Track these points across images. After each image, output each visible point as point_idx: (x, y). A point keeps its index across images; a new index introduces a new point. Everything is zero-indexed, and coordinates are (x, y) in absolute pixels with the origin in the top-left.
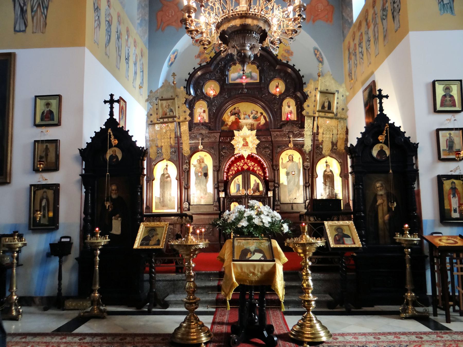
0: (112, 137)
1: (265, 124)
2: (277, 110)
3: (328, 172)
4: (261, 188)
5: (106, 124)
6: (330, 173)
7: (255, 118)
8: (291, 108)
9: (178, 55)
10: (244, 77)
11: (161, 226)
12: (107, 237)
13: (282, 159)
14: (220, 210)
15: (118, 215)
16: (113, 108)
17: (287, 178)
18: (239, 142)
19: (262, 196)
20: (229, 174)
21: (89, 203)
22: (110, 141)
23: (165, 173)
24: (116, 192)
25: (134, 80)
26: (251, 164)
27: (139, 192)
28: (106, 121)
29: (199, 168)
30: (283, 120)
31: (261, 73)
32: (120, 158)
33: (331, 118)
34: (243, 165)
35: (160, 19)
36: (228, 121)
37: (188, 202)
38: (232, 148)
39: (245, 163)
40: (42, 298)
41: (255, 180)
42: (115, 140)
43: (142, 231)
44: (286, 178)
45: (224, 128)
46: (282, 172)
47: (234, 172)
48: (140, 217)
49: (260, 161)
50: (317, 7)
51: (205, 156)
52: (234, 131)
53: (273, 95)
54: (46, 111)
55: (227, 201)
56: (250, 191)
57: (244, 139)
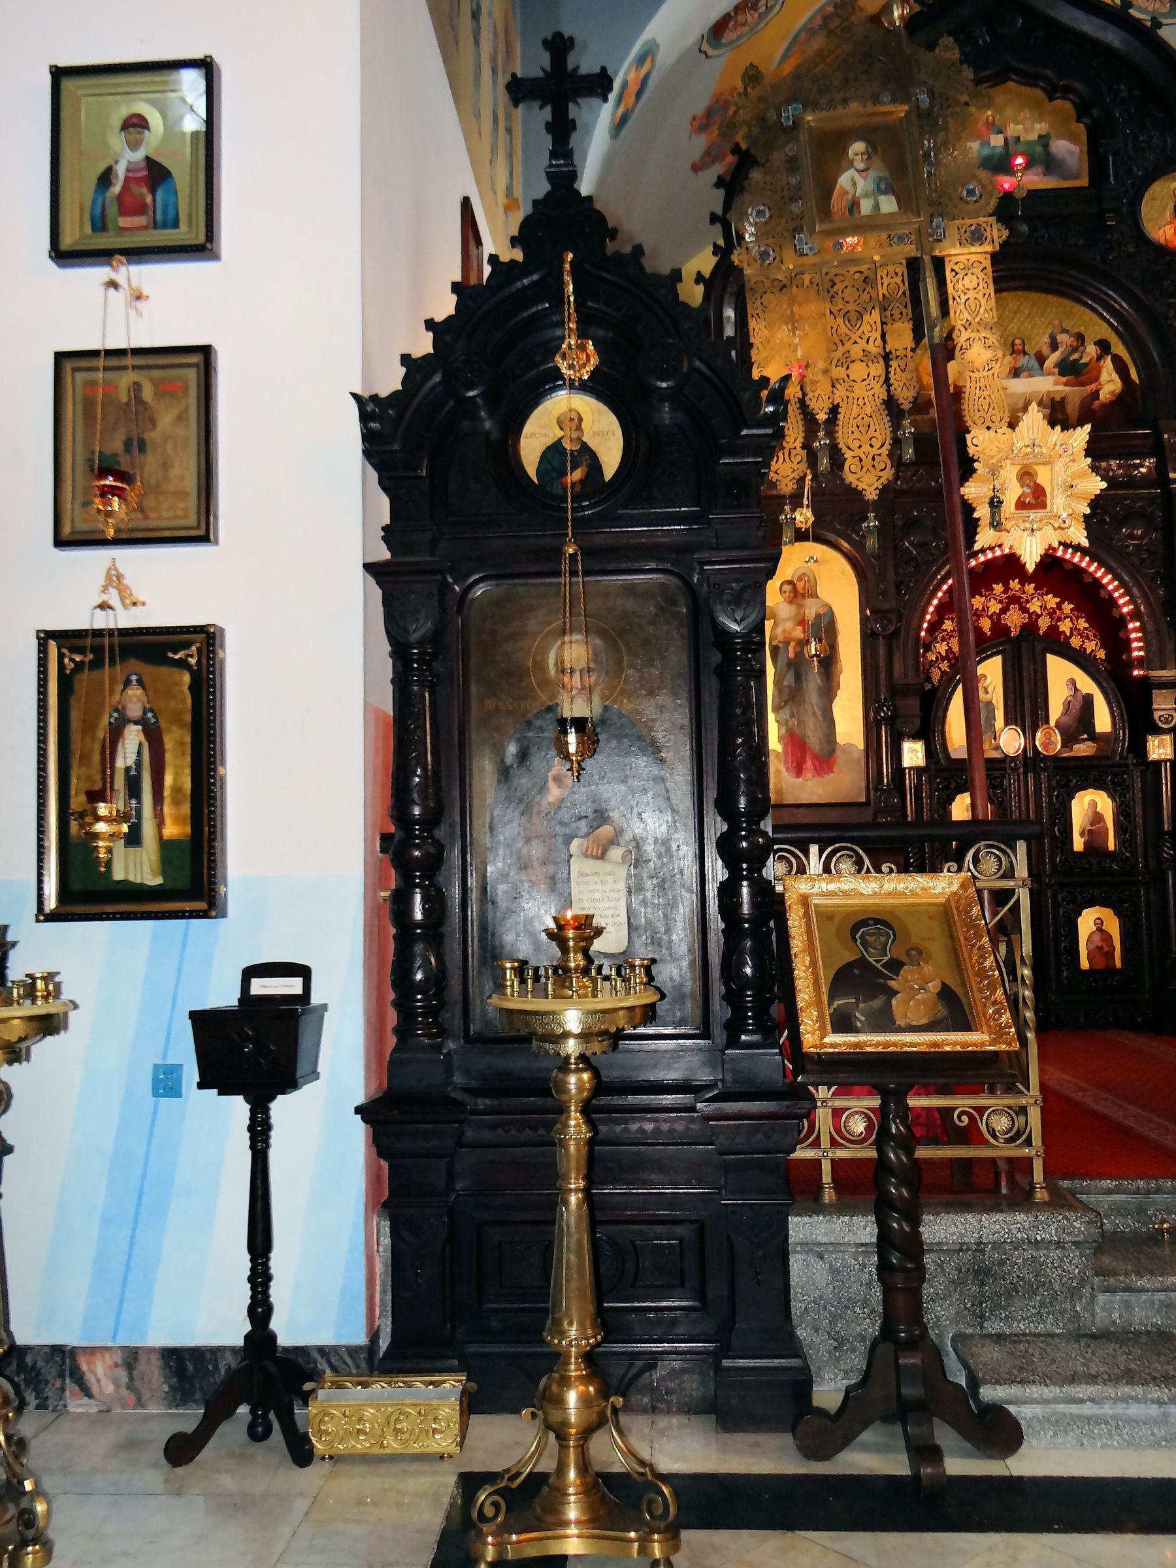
1: (1120, 400)
4: (1103, 721)
7: (1070, 369)
9: (654, 74)
19: (1108, 758)
21: (940, 600)
29: (789, 625)
34: (1004, 610)
39: (1014, 599)
40: (132, 1357)
41: (1073, 682)
49: (1097, 583)
54: (121, 170)
57: (1026, 475)
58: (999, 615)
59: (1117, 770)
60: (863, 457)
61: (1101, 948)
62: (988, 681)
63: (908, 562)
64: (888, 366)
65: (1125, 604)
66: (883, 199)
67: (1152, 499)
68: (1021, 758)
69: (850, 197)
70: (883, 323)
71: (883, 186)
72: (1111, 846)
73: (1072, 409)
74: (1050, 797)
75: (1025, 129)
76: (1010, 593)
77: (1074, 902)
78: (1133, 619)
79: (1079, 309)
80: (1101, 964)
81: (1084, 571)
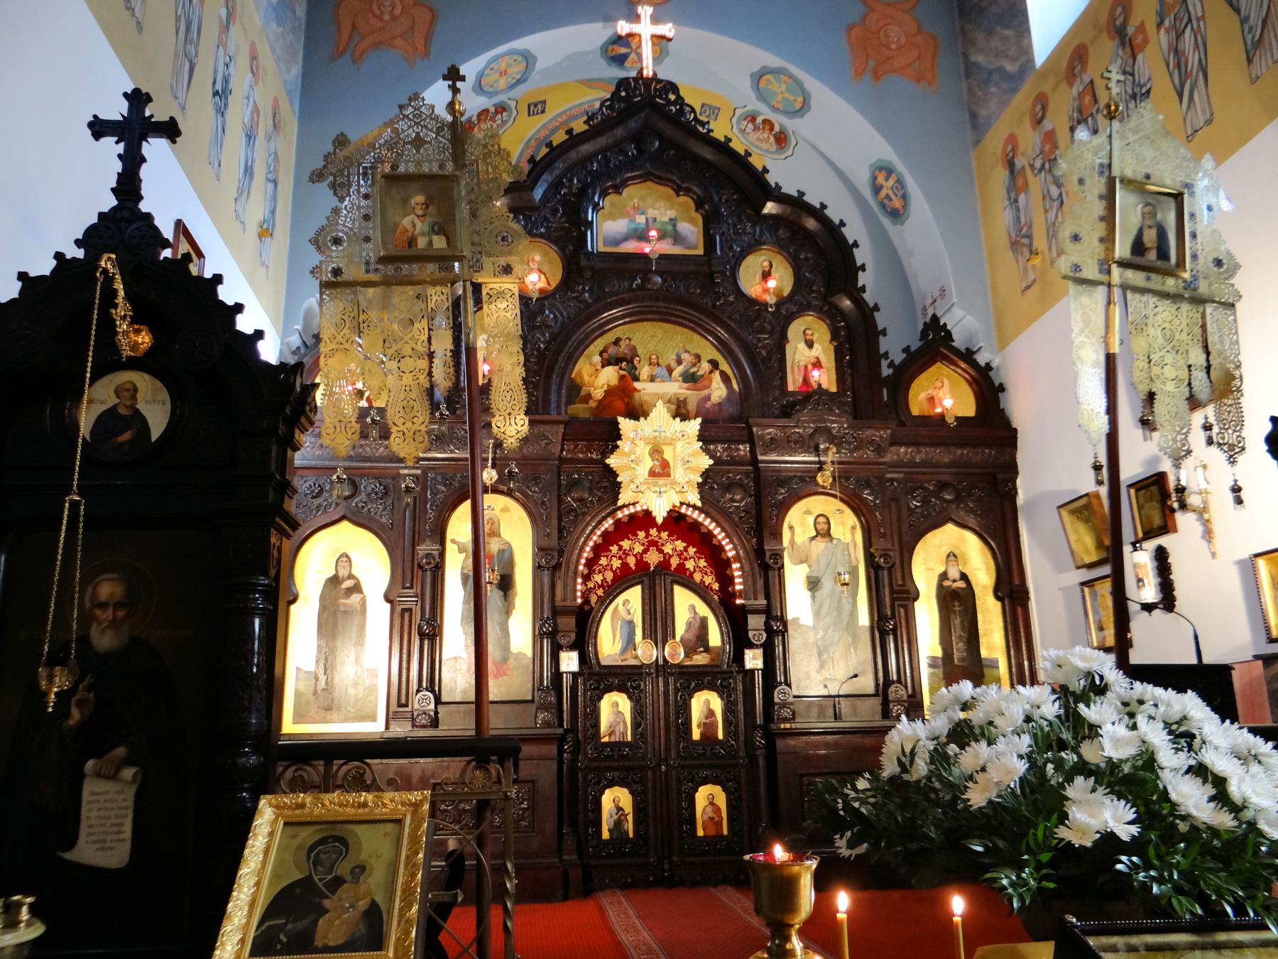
0: (122, 308)
2: (768, 353)
3: (954, 581)
4: (715, 638)
5: (91, 240)
6: (961, 584)
7: (691, 378)
8: (818, 351)
10: (653, 233)
11: (380, 812)
12: (24, 914)
13: (791, 528)
14: (561, 725)
15: (121, 751)
16: (144, 160)
17: (813, 597)
18: (637, 462)
19: (718, 666)
20: (591, 585)
22: (108, 325)
23: (343, 573)
24: (120, 614)
25: (240, 192)
26: (673, 546)
27: (253, 612)
28: (95, 220)
30: (791, 388)
31: (710, 223)
32: (157, 426)
33: (1174, 297)
34: (645, 551)
35: (346, 22)
36: (592, 386)
37: (433, 691)
38: (610, 484)
39: (653, 543)
41: (693, 608)
42: (137, 332)
43: (267, 852)
44: (809, 601)
45: (579, 410)
46: (794, 577)
47: (609, 576)
48: (253, 760)
49: (710, 535)
50: (886, 35)
51: (505, 510)
52: (620, 419)
53: (753, 302)
55: (585, 685)
56: (674, 649)
57: (656, 452)
58: (641, 555)
59: (725, 676)
60: (406, 432)
61: (712, 819)
62: (631, 604)
63: (569, 513)
64: (431, 362)
65: (730, 550)
66: (435, 238)
67: (747, 474)
68: (654, 666)
69: (410, 234)
70: (429, 329)
71: (436, 228)
72: (720, 736)
73: (692, 406)
74: (676, 697)
75: (660, 214)
76: (650, 538)
77: (692, 781)
78: (735, 562)
79: (696, 337)
80: (712, 832)
81: (701, 524)
